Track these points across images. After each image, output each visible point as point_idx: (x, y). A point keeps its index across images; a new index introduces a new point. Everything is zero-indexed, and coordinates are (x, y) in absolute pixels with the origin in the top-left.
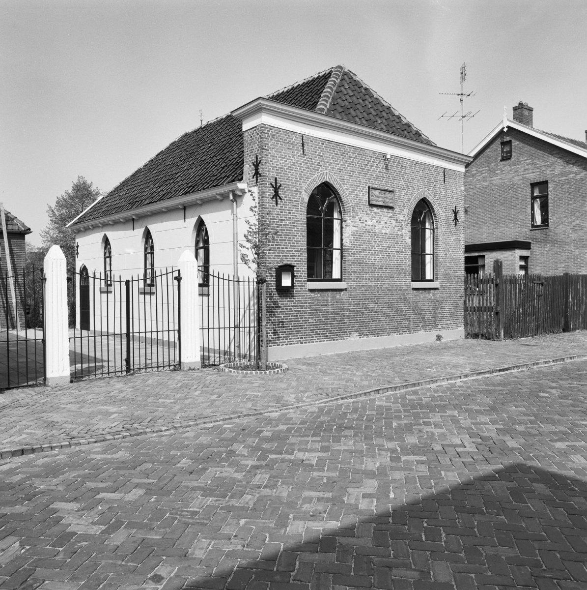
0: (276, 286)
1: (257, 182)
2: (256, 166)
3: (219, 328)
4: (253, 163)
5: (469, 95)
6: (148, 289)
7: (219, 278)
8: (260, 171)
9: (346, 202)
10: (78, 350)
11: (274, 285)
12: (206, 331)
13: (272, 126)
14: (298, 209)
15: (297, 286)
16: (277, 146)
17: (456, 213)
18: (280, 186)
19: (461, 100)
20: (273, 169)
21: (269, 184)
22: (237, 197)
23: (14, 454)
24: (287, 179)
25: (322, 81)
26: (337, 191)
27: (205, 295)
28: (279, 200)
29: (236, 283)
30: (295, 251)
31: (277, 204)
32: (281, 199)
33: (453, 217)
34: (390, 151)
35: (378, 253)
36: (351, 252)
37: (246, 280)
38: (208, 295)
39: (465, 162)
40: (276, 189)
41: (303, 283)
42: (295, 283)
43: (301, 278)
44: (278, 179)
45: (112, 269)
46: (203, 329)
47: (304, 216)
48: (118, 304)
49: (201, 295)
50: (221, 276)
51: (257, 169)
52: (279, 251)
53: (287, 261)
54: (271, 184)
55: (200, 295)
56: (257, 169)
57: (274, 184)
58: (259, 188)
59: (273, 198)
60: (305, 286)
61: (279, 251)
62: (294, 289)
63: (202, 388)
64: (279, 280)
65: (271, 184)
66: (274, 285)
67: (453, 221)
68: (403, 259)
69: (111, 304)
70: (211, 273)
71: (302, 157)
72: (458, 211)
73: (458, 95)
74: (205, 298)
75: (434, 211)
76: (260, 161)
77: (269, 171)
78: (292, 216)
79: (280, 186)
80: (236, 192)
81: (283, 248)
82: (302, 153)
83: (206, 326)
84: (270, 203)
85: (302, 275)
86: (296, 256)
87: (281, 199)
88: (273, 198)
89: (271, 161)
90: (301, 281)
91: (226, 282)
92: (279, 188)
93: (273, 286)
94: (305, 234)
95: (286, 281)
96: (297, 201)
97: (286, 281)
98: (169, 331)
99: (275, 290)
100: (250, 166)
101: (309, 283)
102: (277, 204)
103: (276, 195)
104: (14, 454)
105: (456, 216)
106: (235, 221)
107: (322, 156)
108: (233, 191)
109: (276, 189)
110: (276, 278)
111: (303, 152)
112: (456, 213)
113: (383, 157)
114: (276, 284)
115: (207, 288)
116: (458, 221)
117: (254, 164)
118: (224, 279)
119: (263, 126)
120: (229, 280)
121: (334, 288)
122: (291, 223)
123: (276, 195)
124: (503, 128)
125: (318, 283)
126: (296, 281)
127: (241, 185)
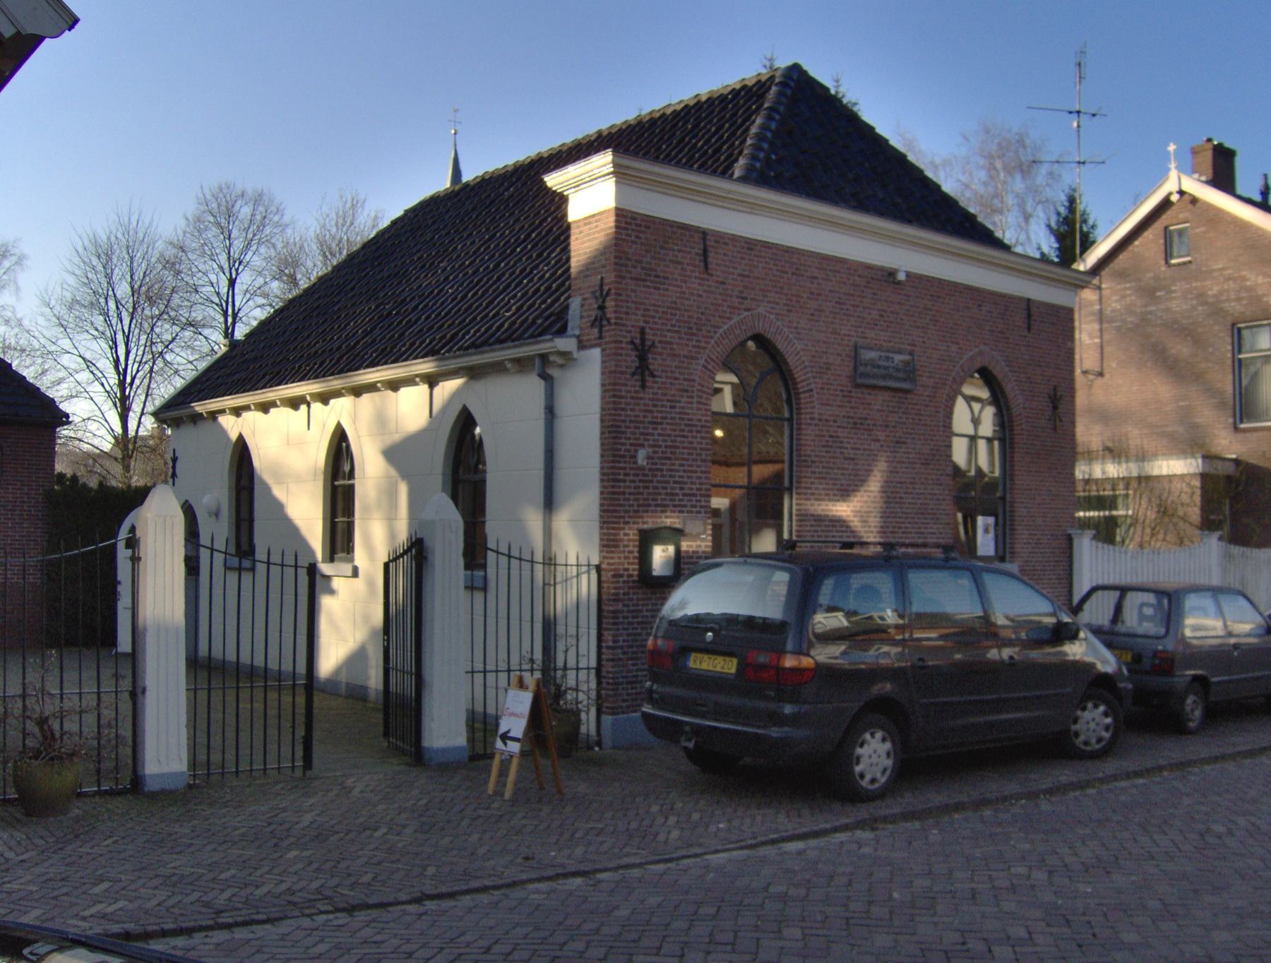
1: (601, 337)
3: (485, 672)
4: (593, 293)
7: (510, 556)
10: (479, 708)
12: (479, 678)
20: (637, 309)
21: (627, 343)
23: (1160, 768)
25: (744, 98)
27: (479, 589)
28: (649, 379)
29: (515, 563)
30: (684, 495)
31: (643, 387)
37: (504, 549)
38: (485, 589)
40: (643, 351)
44: (647, 330)
46: (473, 672)
48: (289, 598)
49: (471, 588)
50: (515, 553)
55: (466, 587)
58: (603, 350)
63: (475, 810)
65: (632, 342)
68: (642, 414)
69: (246, 595)
74: (479, 596)
77: (627, 313)
81: (657, 488)
82: (702, 269)
83: (479, 666)
86: (685, 506)
89: (633, 291)
91: (503, 560)
98: (485, 672)
102: (643, 387)
103: (643, 370)
104: (1160, 768)
107: (748, 277)
118: (520, 559)
120: (532, 562)
123: (643, 370)
124: (1170, 194)
127: (565, 344)
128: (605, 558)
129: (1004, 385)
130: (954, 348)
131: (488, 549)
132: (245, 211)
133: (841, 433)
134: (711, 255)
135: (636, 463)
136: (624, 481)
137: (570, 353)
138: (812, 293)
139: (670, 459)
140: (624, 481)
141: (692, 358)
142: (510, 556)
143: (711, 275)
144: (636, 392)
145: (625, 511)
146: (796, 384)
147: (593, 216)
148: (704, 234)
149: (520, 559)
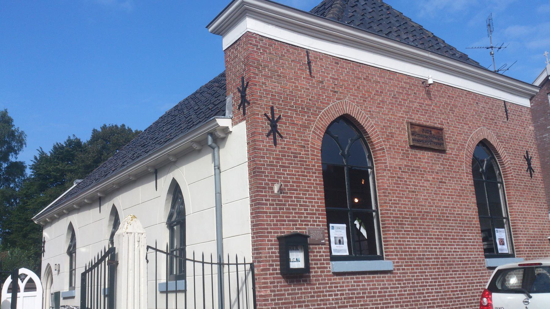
0: (281, 269)
2: (243, 92)
5: (500, 48)
6: (172, 284)
7: (203, 263)
8: (248, 98)
9: (377, 143)
11: (278, 267)
13: (262, 36)
14: (308, 151)
15: (314, 268)
16: (316, 177)
17: (528, 160)
18: (279, 118)
19: (491, 54)
22: (219, 138)
24: (289, 109)
26: (362, 127)
28: (278, 138)
30: (307, 214)
31: (275, 143)
32: (281, 137)
33: (526, 167)
34: (432, 76)
35: (431, 216)
36: (392, 214)
37: (199, 258)
38: (185, 291)
39: (530, 95)
40: (274, 123)
41: (323, 264)
42: (312, 264)
43: (320, 256)
44: (275, 108)
45: (68, 258)
47: (317, 163)
51: (243, 97)
52: (283, 213)
53: (297, 229)
54: (265, 115)
56: (243, 97)
57: (269, 115)
59: (268, 135)
60: (327, 268)
61: (283, 213)
62: (309, 272)
64: (285, 260)
65: (265, 115)
66: (278, 267)
67: (527, 171)
70: (189, 255)
71: (308, 79)
72: (531, 157)
73: (488, 48)
75: (499, 157)
76: (248, 83)
78: (300, 161)
79: (279, 118)
80: (216, 133)
84: (266, 142)
85: (322, 250)
87: (281, 137)
88: (268, 135)
89: (263, 83)
90: (320, 260)
91: (199, 266)
92: (277, 121)
93: (276, 270)
94: (321, 188)
95: (297, 261)
96: (305, 140)
97: (297, 261)
99: (280, 276)
100: (234, 94)
101: (333, 263)
102: (275, 143)
103: (274, 131)
105: (529, 164)
106: (217, 176)
108: (211, 134)
109: (274, 123)
110: (280, 257)
111: (310, 73)
112: (528, 160)
113: (423, 83)
114: (281, 265)
115: (184, 281)
116: (534, 172)
117: (239, 91)
118: (194, 261)
119: (248, 36)
121: (376, 270)
122: (298, 172)
123: (274, 131)
125: (347, 263)
126: (312, 260)
127: (222, 122)
128: (256, 258)
129: (498, 149)
130: (466, 127)
131: (167, 253)
132: (256, 255)
133: (405, 176)
134: (313, 65)
135: (273, 192)
136: (266, 204)
137: (227, 128)
138: (377, 91)
139: (296, 190)
140: (266, 204)
141: (306, 127)
142: (203, 263)
143: (314, 77)
144: (270, 146)
145: (268, 225)
146: (373, 145)
147: (236, 42)
148: (308, 52)
149: (194, 261)
